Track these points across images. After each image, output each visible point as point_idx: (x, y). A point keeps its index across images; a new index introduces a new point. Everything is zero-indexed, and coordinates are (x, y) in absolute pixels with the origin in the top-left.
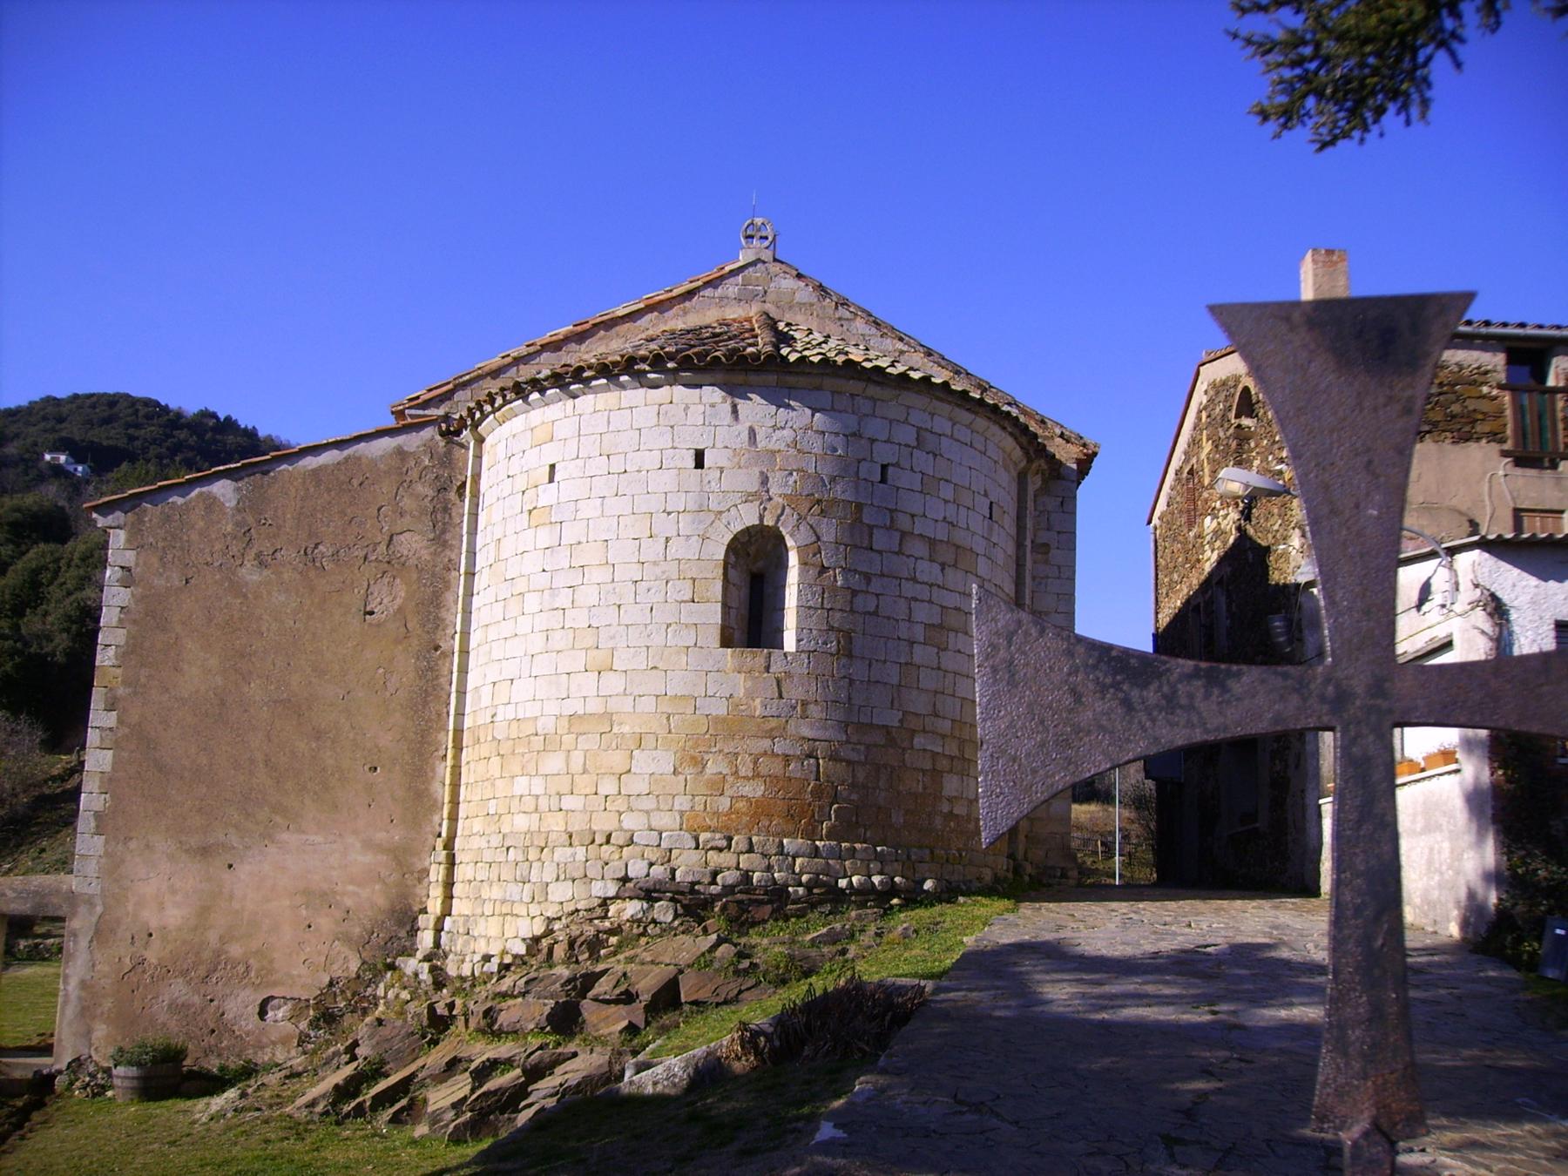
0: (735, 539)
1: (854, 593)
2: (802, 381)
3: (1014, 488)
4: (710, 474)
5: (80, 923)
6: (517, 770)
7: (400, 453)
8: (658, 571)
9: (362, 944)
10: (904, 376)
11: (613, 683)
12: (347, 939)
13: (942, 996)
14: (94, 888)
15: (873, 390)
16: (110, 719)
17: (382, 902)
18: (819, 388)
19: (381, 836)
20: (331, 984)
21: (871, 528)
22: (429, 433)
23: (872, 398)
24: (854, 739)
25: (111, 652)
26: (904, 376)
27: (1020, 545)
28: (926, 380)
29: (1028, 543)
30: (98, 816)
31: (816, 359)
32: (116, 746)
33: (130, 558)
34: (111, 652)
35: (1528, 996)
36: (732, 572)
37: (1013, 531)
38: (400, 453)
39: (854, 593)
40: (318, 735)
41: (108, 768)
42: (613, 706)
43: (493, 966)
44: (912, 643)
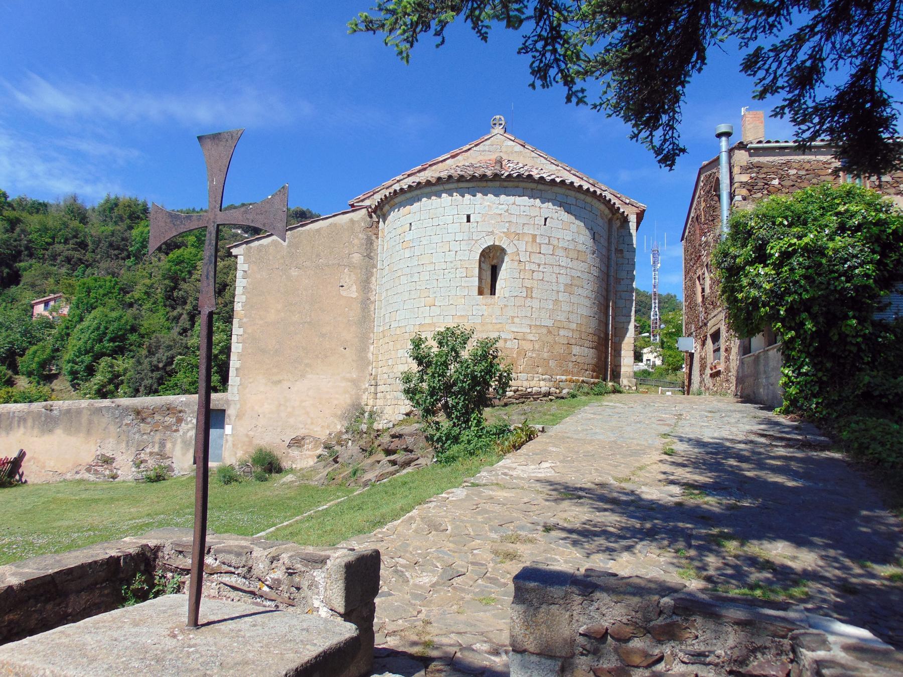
0: (483, 251)
1: (533, 272)
2: (511, 184)
3: (606, 226)
4: (473, 224)
5: (231, 412)
6: (399, 347)
7: (352, 221)
8: (452, 265)
9: (343, 417)
10: (553, 180)
11: (436, 311)
12: (335, 415)
13: (768, 461)
14: (237, 398)
15: (540, 187)
16: (241, 331)
17: (349, 401)
18: (517, 187)
19: (348, 375)
20: (330, 434)
21: (540, 244)
22: (364, 211)
23: (541, 190)
24: (534, 331)
25: (240, 304)
26: (553, 180)
27: (609, 250)
28: (563, 182)
29: (613, 249)
30: (237, 369)
31: (515, 175)
32: (243, 342)
33: (246, 267)
34: (240, 304)
35: (22, 264)
36: (482, 265)
37: (606, 244)
38: (352, 221)
39: (533, 272)
40: (323, 335)
41: (240, 351)
42: (435, 320)
43: (391, 425)
44: (558, 292)
